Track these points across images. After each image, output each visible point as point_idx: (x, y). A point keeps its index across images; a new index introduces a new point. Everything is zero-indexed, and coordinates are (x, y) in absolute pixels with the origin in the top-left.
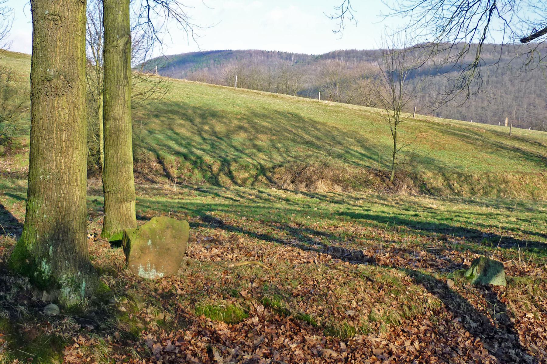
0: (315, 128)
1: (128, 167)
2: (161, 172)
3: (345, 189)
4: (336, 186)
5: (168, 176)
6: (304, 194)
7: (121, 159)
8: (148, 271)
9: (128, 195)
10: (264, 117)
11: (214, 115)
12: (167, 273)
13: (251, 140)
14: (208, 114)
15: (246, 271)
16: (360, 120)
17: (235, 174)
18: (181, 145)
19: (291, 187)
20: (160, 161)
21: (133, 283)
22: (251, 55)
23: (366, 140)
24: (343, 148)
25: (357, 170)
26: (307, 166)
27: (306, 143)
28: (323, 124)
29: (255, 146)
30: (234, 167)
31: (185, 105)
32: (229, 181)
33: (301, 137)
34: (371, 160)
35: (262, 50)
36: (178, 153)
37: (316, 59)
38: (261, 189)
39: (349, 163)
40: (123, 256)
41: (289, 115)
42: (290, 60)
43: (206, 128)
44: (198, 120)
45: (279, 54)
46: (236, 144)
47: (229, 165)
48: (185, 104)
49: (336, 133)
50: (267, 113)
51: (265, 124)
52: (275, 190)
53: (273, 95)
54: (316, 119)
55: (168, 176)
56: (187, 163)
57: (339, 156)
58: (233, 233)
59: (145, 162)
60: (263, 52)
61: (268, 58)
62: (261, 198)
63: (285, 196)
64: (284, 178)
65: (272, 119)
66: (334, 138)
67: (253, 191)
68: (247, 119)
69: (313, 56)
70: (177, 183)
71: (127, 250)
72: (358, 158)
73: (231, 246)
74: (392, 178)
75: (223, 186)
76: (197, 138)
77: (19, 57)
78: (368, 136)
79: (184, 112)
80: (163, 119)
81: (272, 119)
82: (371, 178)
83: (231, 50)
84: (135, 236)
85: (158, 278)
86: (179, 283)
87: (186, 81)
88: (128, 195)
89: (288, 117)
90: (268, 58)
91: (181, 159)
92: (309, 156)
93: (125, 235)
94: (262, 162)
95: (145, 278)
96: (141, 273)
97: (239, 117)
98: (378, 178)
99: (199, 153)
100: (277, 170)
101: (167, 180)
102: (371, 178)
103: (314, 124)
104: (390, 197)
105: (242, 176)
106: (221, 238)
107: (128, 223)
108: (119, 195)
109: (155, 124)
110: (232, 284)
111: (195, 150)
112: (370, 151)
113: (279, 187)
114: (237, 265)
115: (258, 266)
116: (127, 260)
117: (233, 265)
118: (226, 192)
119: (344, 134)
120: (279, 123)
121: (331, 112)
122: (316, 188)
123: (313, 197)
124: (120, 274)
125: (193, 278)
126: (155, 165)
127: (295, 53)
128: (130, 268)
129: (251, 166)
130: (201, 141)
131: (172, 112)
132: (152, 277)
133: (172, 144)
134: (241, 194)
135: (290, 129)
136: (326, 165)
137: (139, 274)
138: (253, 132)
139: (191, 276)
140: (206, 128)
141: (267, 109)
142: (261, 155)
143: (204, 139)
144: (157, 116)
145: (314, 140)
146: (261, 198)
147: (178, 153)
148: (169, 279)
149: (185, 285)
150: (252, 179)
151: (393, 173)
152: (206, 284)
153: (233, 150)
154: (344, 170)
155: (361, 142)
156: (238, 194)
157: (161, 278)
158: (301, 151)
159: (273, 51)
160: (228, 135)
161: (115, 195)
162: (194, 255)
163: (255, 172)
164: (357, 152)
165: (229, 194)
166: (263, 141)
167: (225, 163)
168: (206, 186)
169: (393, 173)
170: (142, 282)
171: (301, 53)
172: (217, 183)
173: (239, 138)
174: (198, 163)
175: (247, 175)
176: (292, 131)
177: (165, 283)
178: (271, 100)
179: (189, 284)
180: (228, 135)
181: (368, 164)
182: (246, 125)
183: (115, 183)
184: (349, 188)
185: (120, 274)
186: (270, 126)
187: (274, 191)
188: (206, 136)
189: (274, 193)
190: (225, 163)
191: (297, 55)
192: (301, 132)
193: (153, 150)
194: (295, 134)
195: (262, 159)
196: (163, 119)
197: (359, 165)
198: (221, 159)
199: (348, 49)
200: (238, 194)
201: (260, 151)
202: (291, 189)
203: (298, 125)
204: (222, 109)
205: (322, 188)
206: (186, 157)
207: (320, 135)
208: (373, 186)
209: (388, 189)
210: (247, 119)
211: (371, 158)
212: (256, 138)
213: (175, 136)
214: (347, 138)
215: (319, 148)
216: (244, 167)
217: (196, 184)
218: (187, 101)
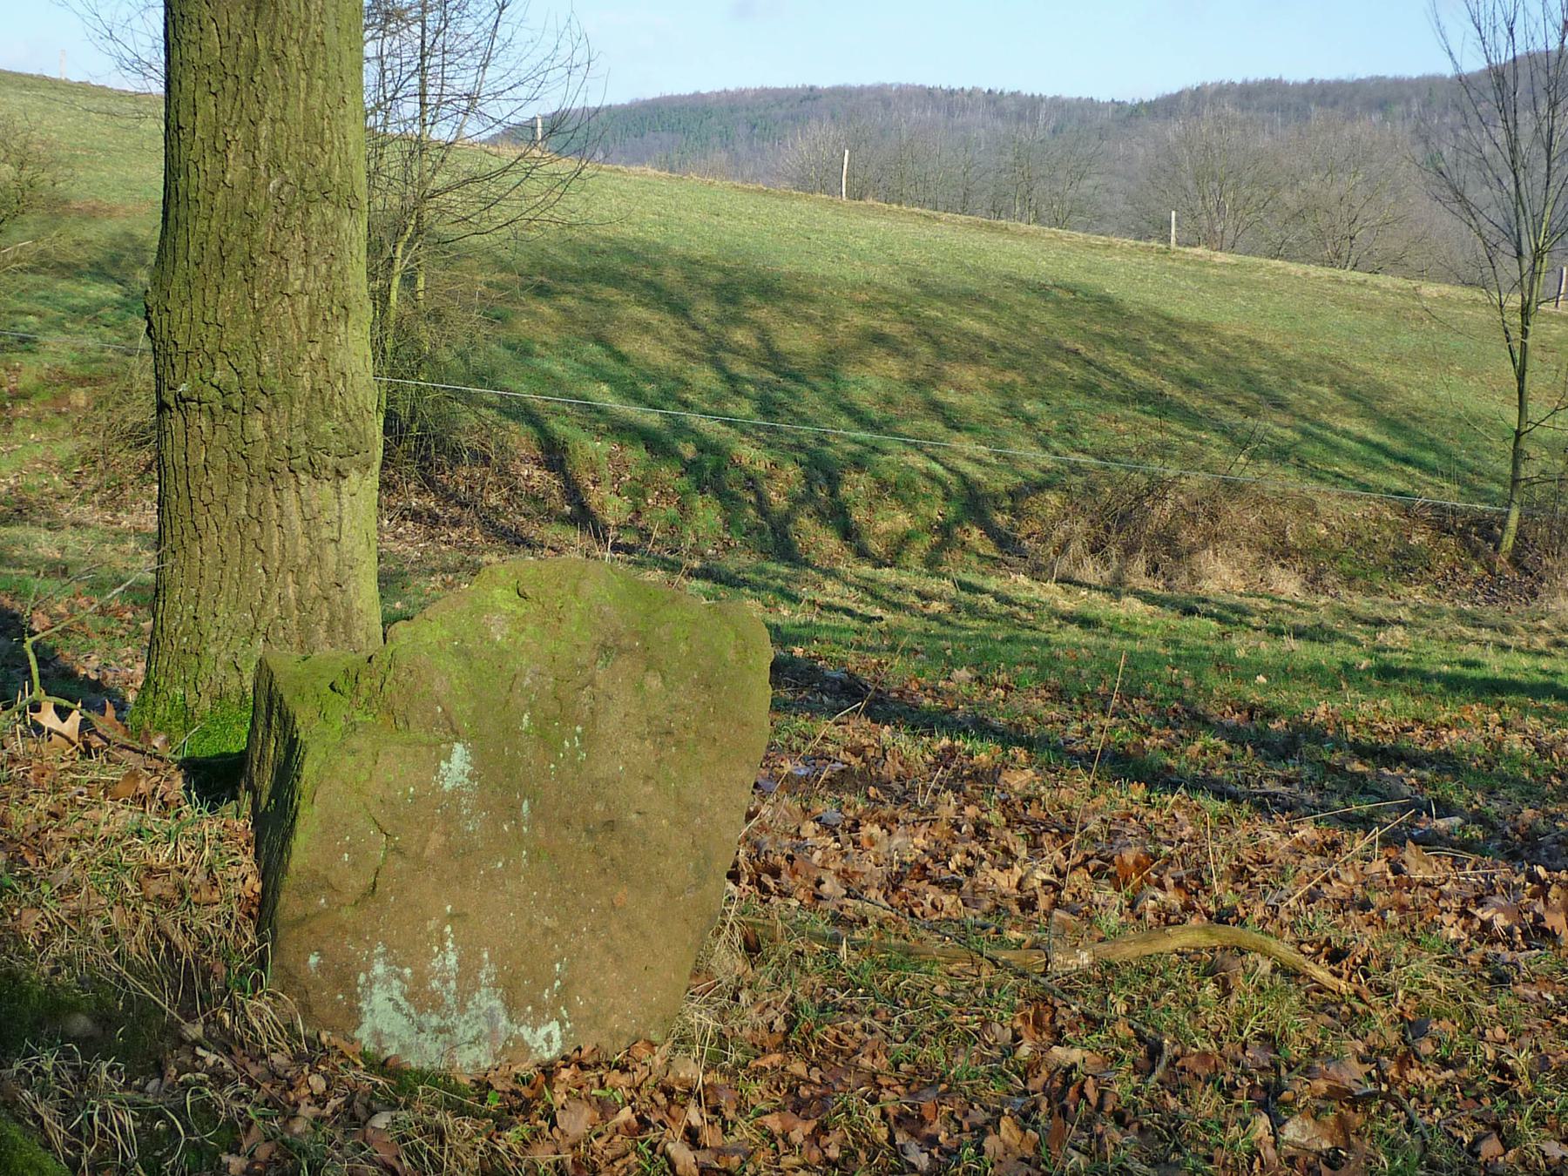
0: (1171, 339)
1: (328, 227)
2: (556, 500)
3: (1314, 582)
4: (1275, 571)
5: (584, 517)
6: (1148, 598)
7: (275, 162)
8: (437, 1004)
9: (326, 427)
10: (968, 298)
11: (768, 289)
12: (595, 1019)
13: (917, 384)
14: (742, 288)
15: (1192, 1007)
16: (1345, 316)
17: (859, 515)
18: (638, 397)
19: (1091, 571)
20: (554, 455)
21: (299, 1126)
22: (887, 103)
23: (1383, 392)
24: (1286, 421)
25: (1357, 511)
26: (1157, 488)
27: (1144, 397)
28: (1203, 329)
29: (936, 408)
30: (856, 486)
31: (647, 250)
32: (830, 542)
33: (1116, 375)
34: (1409, 469)
35: (929, 84)
36: (623, 430)
37: (1130, 116)
38: (968, 578)
39: (1321, 479)
40: (245, 877)
41: (1062, 294)
42: (1034, 120)
43: (740, 336)
44: (705, 310)
45: (992, 98)
46: (861, 398)
47: (833, 481)
48: (648, 247)
49: (1255, 363)
50: (972, 283)
51: (968, 323)
52: (1023, 580)
53: (989, 225)
54: (1173, 311)
55: (584, 517)
56: (666, 472)
57: (1280, 454)
58: (946, 741)
59: (486, 460)
60: (930, 93)
61: (951, 114)
62: (972, 611)
63: (1082, 603)
64: (1059, 534)
65: (995, 305)
66: (1250, 381)
67: (933, 585)
68: (897, 307)
69: (1120, 105)
70: (616, 548)
71: (273, 831)
72: (1352, 457)
73: (971, 811)
74: (1508, 542)
75: (807, 564)
76: (704, 377)
77: (33, 87)
78: (1385, 374)
79: (646, 274)
80: (568, 301)
81: (995, 305)
82: (1416, 540)
83: (812, 89)
84: (339, 709)
85: (526, 1068)
86: (694, 1115)
87: (651, 172)
88: (326, 427)
89: (1058, 302)
90: (951, 114)
91: (637, 454)
92: (1164, 450)
93: (270, 706)
94: (969, 468)
95: (413, 1061)
96: (384, 1019)
97: (864, 297)
98: (1450, 541)
99: (709, 427)
100: (1031, 503)
101: (574, 535)
102: (1416, 540)
103: (1170, 328)
104: (1517, 613)
105: (884, 526)
106: (891, 768)
107: (322, 633)
108: (256, 426)
109: (538, 321)
110: (1120, 1119)
111: (693, 419)
112: (1408, 438)
113: (1037, 572)
114: (1116, 958)
115: (1265, 967)
116: (263, 910)
117: (1085, 958)
118: (820, 588)
119: (1289, 364)
120: (1024, 321)
121: (1222, 283)
122: (1195, 578)
123: (1189, 611)
124: (195, 1031)
125: (798, 1068)
126: (534, 476)
127: (1049, 94)
128: (289, 980)
129: (920, 482)
130: (718, 387)
131: (597, 275)
132: (471, 1060)
133: (603, 395)
134: (886, 594)
135: (1069, 344)
136: (1233, 488)
137: (363, 1034)
138: (925, 351)
139: (784, 1046)
140: (740, 336)
141: (975, 270)
142: (965, 444)
143: (732, 379)
144: (542, 291)
145: (1169, 388)
146: (972, 611)
147: (623, 430)
148: (614, 1077)
149: (744, 1131)
150: (928, 540)
151: (1513, 522)
152: (910, 1121)
153: (844, 420)
154: (1308, 507)
155: (1365, 400)
156: (870, 590)
157: (548, 1071)
158: (1125, 428)
159: (968, 88)
160: (830, 365)
161: (234, 421)
162: (775, 873)
163: (937, 511)
164: (1346, 434)
165: (833, 591)
166: (967, 388)
167: (823, 471)
168: (740, 561)
169: (1513, 522)
170: (381, 1121)
171: (1075, 95)
172: (784, 548)
173: (872, 380)
174: (711, 473)
175: (902, 520)
176: (1076, 352)
177: (577, 1121)
178: (981, 240)
179: (773, 1123)
180: (830, 365)
181: (1399, 484)
182: (892, 329)
183: (230, 334)
184: (1329, 579)
185: (195, 1031)
186: (986, 331)
187: (1020, 584)
188: (741, 368)
189: (1025, 594)
190: (823, 471)
191: (1058, 104)
192: (1111, 358)
193: (529, 416)
194: (1090, 363)
195: (968, 454)
196: (568, 301)
197: (1365, 487)
198: (803, 457)
199: (1251, 79)
200: (870, 590)
201: (954, 425)
202: (1091, 580)
203: (1097, 328)
204: (793, 268)
205: (1220, 576)
206: (652, 442)
207: (1189, 366)
208: (1431, 576)
209: (1493, 587)
210: (897, 307)
211: (1407, 461)
212: (937, 378)
213: (611, 365)
214: (1300, 384)
215: (1193, 419)
216: (897, 491)
217: (696, 551)
218: (655, 235)
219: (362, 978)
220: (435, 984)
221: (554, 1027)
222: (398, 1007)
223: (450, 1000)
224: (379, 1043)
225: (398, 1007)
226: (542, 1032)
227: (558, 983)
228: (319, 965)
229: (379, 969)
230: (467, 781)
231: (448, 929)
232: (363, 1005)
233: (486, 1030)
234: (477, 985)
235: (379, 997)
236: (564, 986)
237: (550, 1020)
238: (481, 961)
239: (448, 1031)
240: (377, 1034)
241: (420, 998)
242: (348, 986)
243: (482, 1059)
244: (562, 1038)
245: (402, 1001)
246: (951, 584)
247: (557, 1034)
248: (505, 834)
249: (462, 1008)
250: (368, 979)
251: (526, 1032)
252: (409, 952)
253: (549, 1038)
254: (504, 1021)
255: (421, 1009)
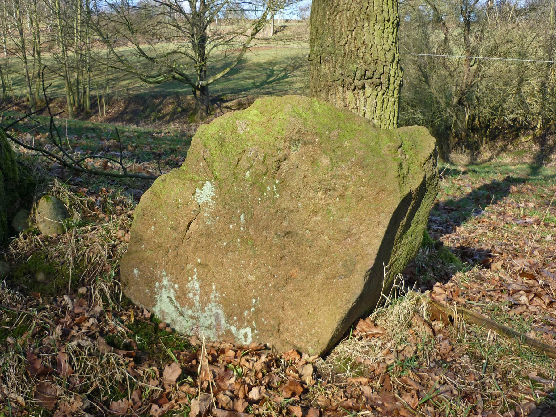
219: (157, 284)
220: (191, 295)
221: (248, 330)
222: (171, 300)
223: (197, 304)
224: (163, 316)
225: (171, 300)
226: (243, 331)
227: (253, 309)
228: (138, 275)
229: (165, 282)
230: (210, 200)
231: (195, 270)
232: (158, 297)
233: (214, 323)
234: (209, 301)
235: (165, 295)
236: (255, 312)
237: (247, 326)
238: (212, 289)
239: (195, 319)
240: (162, 311)
241: (182, 297)
242: (151, 287)
243: (211, 336)
244: (252, 337)
245: (173, 299)
246: (551, 224)
247: (250, 335)
248: (230, 229)
249: (203, 310)
250: (160, 286)
251: (233, 329)
252: (180, 276)
253: (246, 335)
254: (223, 321)
255: (183, 305)
